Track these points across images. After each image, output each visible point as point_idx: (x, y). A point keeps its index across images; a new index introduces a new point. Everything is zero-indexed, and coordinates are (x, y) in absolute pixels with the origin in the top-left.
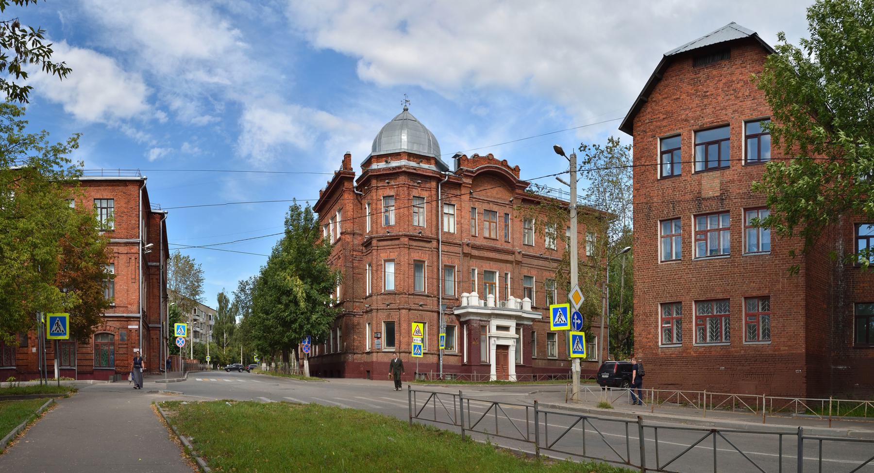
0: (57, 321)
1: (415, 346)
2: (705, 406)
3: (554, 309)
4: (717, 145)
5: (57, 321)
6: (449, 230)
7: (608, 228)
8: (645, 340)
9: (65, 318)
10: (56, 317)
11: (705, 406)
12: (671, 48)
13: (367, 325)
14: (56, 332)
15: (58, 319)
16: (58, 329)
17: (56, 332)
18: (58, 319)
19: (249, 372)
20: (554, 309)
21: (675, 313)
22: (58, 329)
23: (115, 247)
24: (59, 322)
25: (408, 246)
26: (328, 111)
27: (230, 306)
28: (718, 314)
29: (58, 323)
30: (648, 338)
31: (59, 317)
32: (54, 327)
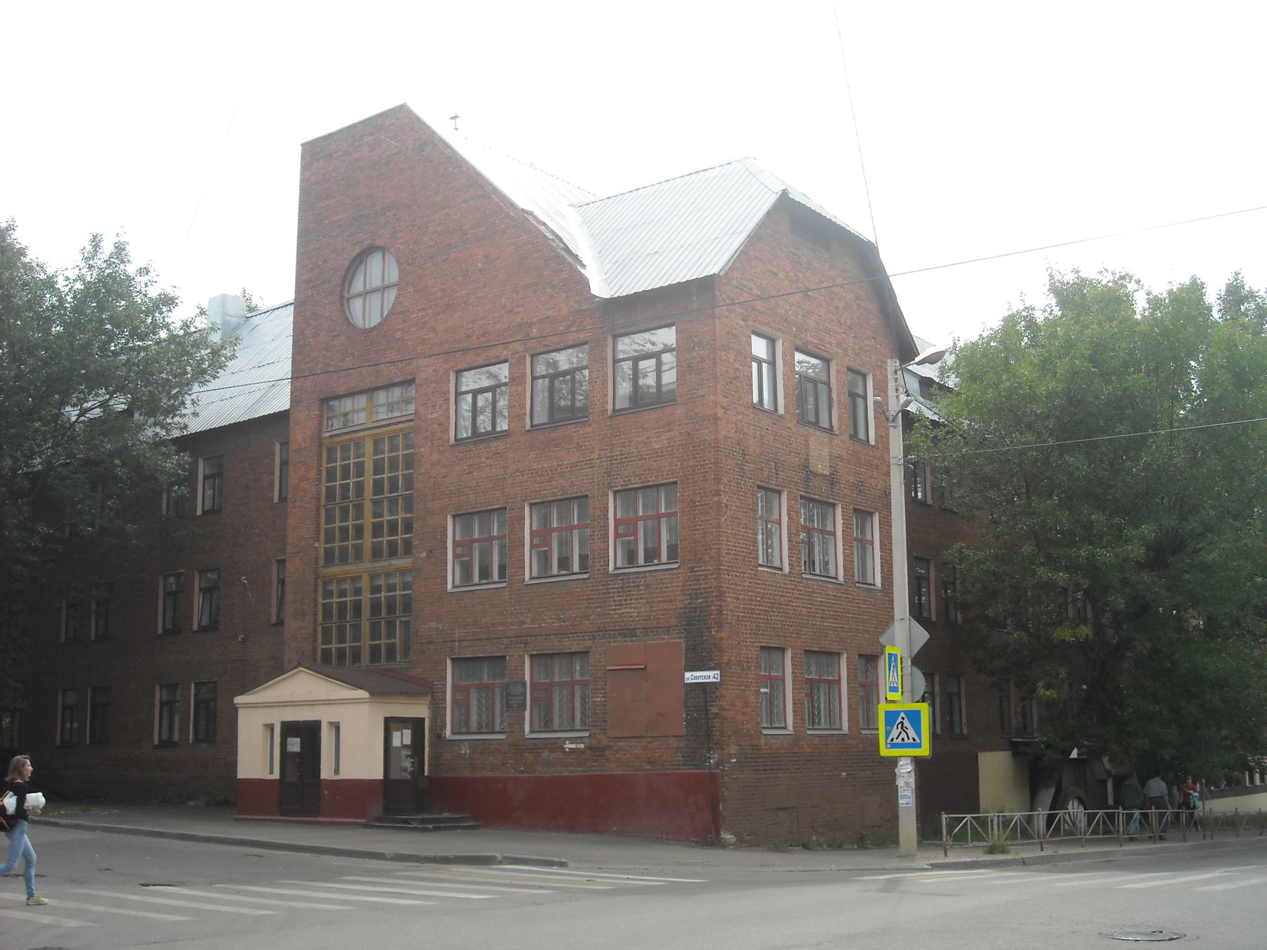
0: (900, 720)
3: (919, 712)
5: (900, 720)
6: (654, 371)
9: (918, 713)
10: (898, 713)
12: (891, 261)
14: (899, 740)
15: (902, 715)
16: (903, 735)
17: (899, 740)
18: (902, 715)
20: (919, 712)
22: (903, 735)
23: (512, 775)
24: (906, 723)
25: (763, 768)
26: (1203, 295)
27: (1216, 314)
28: (491, 681)
29: (902, 723)
32: (895, 732)
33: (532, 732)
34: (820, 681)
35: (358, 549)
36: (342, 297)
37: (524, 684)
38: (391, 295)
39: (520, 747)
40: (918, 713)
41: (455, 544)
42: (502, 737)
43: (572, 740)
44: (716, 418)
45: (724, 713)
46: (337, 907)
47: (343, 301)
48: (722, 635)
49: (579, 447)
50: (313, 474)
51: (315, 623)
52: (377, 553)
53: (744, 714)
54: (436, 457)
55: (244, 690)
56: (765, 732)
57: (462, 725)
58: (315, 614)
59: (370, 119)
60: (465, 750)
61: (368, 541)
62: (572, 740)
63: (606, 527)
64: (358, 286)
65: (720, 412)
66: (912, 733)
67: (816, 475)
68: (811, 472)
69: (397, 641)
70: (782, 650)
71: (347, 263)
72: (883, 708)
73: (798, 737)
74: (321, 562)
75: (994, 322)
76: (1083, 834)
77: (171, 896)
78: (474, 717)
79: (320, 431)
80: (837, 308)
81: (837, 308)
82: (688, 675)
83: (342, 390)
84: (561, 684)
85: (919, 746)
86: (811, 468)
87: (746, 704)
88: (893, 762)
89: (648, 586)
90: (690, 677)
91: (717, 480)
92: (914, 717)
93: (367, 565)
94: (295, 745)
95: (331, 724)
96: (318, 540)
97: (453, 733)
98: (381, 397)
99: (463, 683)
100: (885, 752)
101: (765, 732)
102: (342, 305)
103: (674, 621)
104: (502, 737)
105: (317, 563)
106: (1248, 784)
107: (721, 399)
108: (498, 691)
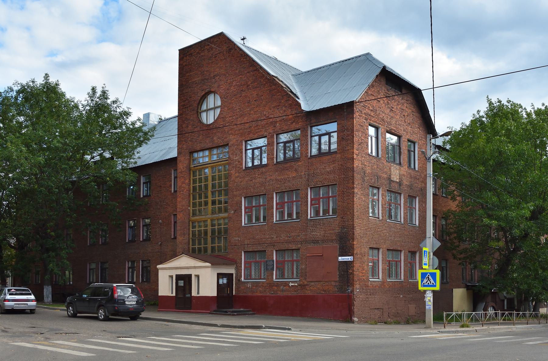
0: (427, 276)
1: (423, 275)
2: (218, 227)
4: (327, 136)
5: (427, 276)
7: (88, 230)
8: (361, 274)
11: (218, 227)
13: (141, 261)
15: (429, 274)
16: (429, 282)
18: (429, 274)
19: (520, 104)
21: (258, 258)
22: (429, 282)
24: (430, 277)
29: (428, 277)
30: (363, 273)
31: (430, 273)
32: (425, 281)
33: (276, 279)
36: (198, 112)
37: (273, 261)
38: (218, 111)
39: (272, 285)
41: (245, 208)
50: (187, 181)
54: (237, 174)
57: (246, 277)
58: (189, 235)
60: (249, 285)
62: (292, 282)
64: (204, 107)
67: (393, 182)
80: (404, 116)
81: (404, 116)
82: (340, 258)
83: (198, 149)
84: (288, 261)
85: (435, 286)
87: (363, 269)
88: (425, 292)
91: (353, 183)
95: (196, 275)
97: (244, 279)
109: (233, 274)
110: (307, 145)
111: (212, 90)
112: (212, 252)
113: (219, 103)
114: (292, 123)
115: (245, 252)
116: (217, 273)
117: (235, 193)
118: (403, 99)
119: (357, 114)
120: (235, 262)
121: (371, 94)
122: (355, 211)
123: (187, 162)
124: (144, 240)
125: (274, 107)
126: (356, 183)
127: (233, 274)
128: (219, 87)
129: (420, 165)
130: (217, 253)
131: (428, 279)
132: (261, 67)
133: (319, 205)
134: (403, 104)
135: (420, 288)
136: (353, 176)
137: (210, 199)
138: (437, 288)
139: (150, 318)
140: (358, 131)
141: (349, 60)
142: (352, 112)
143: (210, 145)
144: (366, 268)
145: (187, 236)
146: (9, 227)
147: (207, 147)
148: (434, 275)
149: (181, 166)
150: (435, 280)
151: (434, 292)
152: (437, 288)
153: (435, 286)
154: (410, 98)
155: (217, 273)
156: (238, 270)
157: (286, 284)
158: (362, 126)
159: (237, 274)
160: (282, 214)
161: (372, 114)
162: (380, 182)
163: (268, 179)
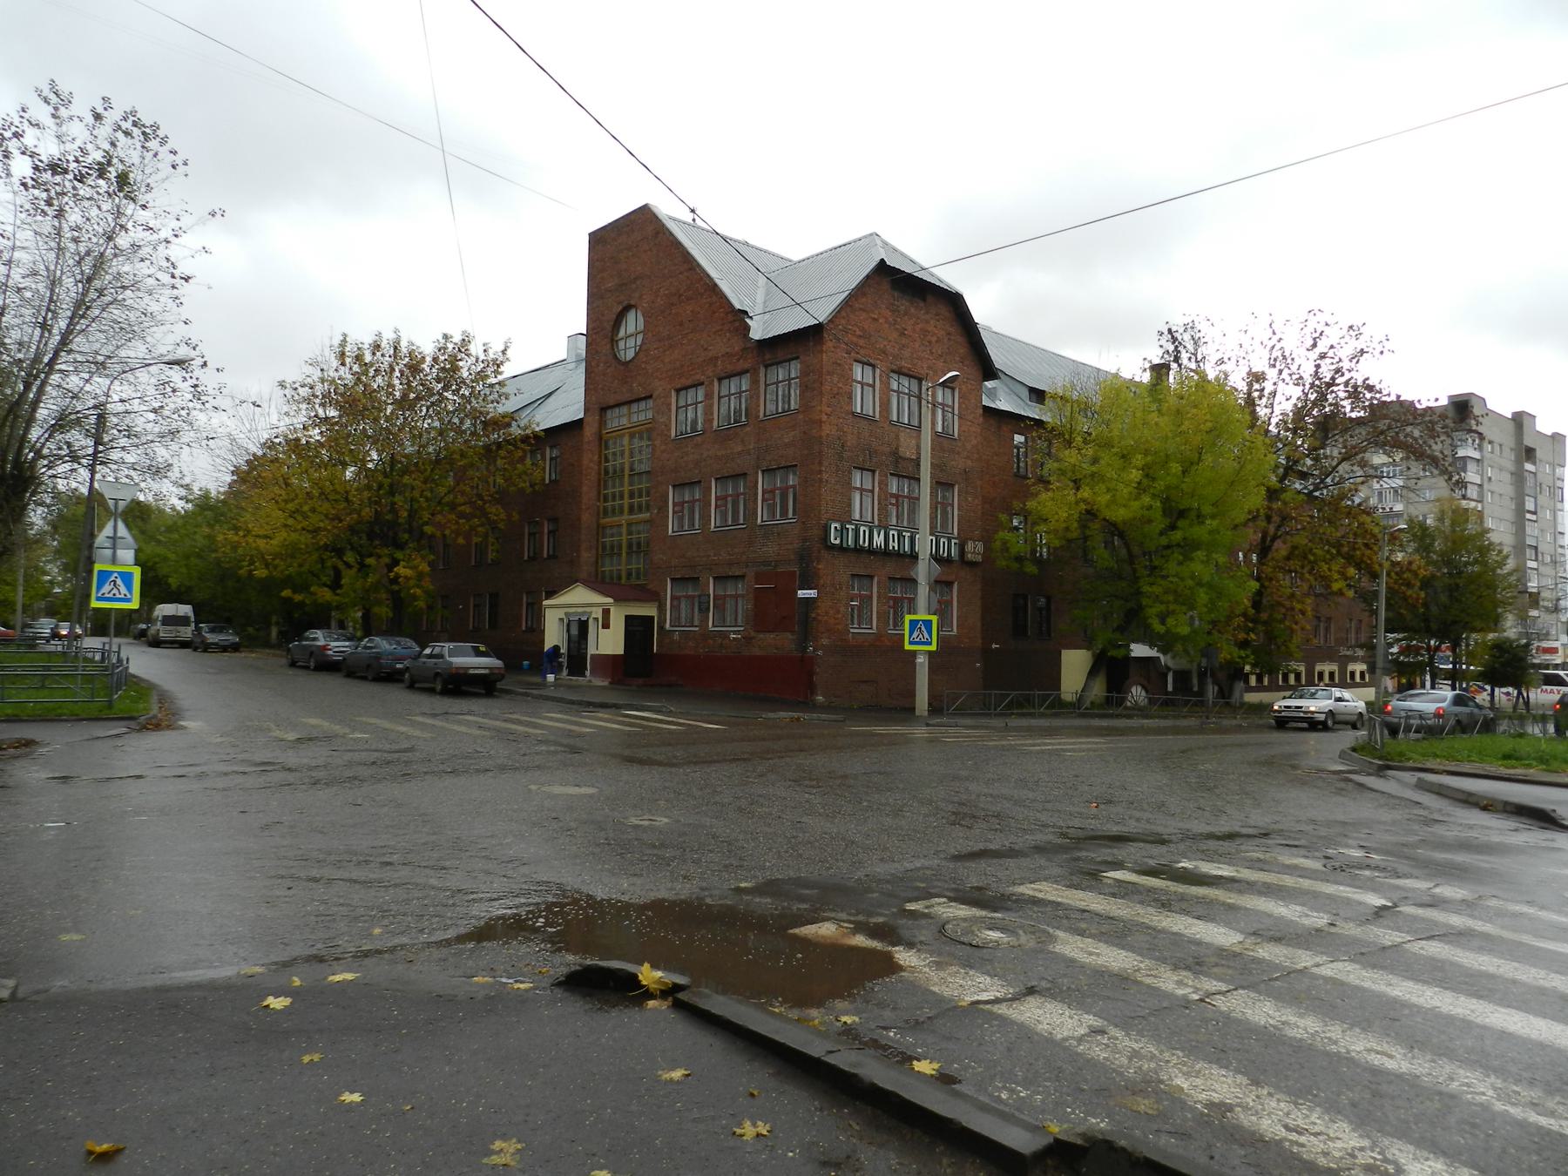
0: (113, 578)
1: (913, 623)
14: (111, 595)
16: (115, 591)
18: (116, 575)
22: (115, 591)
24: (119, 581)
33: (714, 626)
34: (902, 599)
35: (621, 507)
36: (612, 340)
37: (709, 596)
38: (640, 338)
39: (706, 635)
40: (131, 575)
41: (675, 504)
42: (697, 629)
43: (735, 633)
44: (821, 422)
45: (820, 618)
46: (557, 724)
47: (613, 341)
48: (820, 567)
49: (742, 441)
50: (596, 458)
51: (597, 554)
52: (631, 510)
53: (836, 619)
54: (663, 447)
55: (550, 595)
56: (852, 630)
57: (676, 621)
58: (597, 549)
59: (627, 215)
60: (676, 637)
61: (626, 501)
62: (735, 633)
63: (756, 494)
64: (622, 333)
65: (824, 418)
66: (926, 635)
67: (904, 459)
68: (900, 457)
69: (641, 566)
70: (871, 577)
71: (615, 316)
72: (97, 567)
73: (879, 636)
74: (601, 516)
75: (1410, 399)
76: (993, 707)
77: (589, 718)
78: (683, 615)
79: (600, 431)
80: (930, 342)
81: (930, 342)
82: (799, 592)
83: (612, 402)
84: (731, 596)
85: (930, 644)
86: (901, 454)
87: (838, 612)
88: (914, 654)
89: (779, 534)
90: (801, 593)
91: (820, 464)
92: (928, 624)
93: (626, 517)
94: (575, 631)
95: (594, 618)
96: (599, 501)
97: (671, 626)
98: (634, 407)
99: (678, 594)
100: (907, 647)
101: (852, 630)
102: (613, 345)
103: (792, 557)
104: (697, 629)
105: (598, 514)
106: (1280, 683)
107: (825, 408)
108: (696, 600)
109: (653, 617)
110: (758, 397)
111: (632, 302)
112: (628, 579)
113: (641, 326)
114: (738, 360)
115: (672, 579)
116: (626, 616)
117: (659, 478)
118: (927, 313)
119: (830, 344)
120: (655, 597)
121: (861, 309)
122: (823, 512)
123: (596, 425)
124: (549, 557)
125: (715, 333)
126: (825, 463)
127: (653, 617)
128: (640, 297)
129: (962, 429)
130: (634, 581)
131: (115, 585)
132: (699, 265)
133: (774, 499)
134: (927, 322)
135: (907, 647)
136: (820, 452)
137: (626, 489)
138: (933, 648)
139: (1088, 736)
140: (830, 373)
141: (855, 241)
142: (822, 337)
143: (627, 397)
144: (842, 609)
145: (594, 551)
146: (1005, 554)
147: (624, 400)
148: (928, 624)
149: (589, 432)
150: (129, 588)
151: (930, 653)
152: (933, 648)
153: (930, 644)
154: (944, 311)
155: (626, 616)
156: (661, 609)
157: (724, 635)
158: (839, 365)
159: (659, 617)
160: (724, 516)
161: (861, 342)
162: (874, 460)
163: (705, 456)
